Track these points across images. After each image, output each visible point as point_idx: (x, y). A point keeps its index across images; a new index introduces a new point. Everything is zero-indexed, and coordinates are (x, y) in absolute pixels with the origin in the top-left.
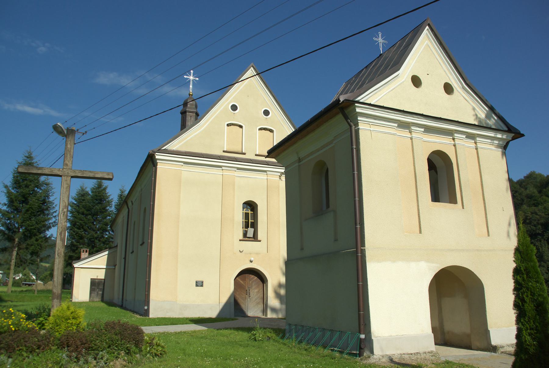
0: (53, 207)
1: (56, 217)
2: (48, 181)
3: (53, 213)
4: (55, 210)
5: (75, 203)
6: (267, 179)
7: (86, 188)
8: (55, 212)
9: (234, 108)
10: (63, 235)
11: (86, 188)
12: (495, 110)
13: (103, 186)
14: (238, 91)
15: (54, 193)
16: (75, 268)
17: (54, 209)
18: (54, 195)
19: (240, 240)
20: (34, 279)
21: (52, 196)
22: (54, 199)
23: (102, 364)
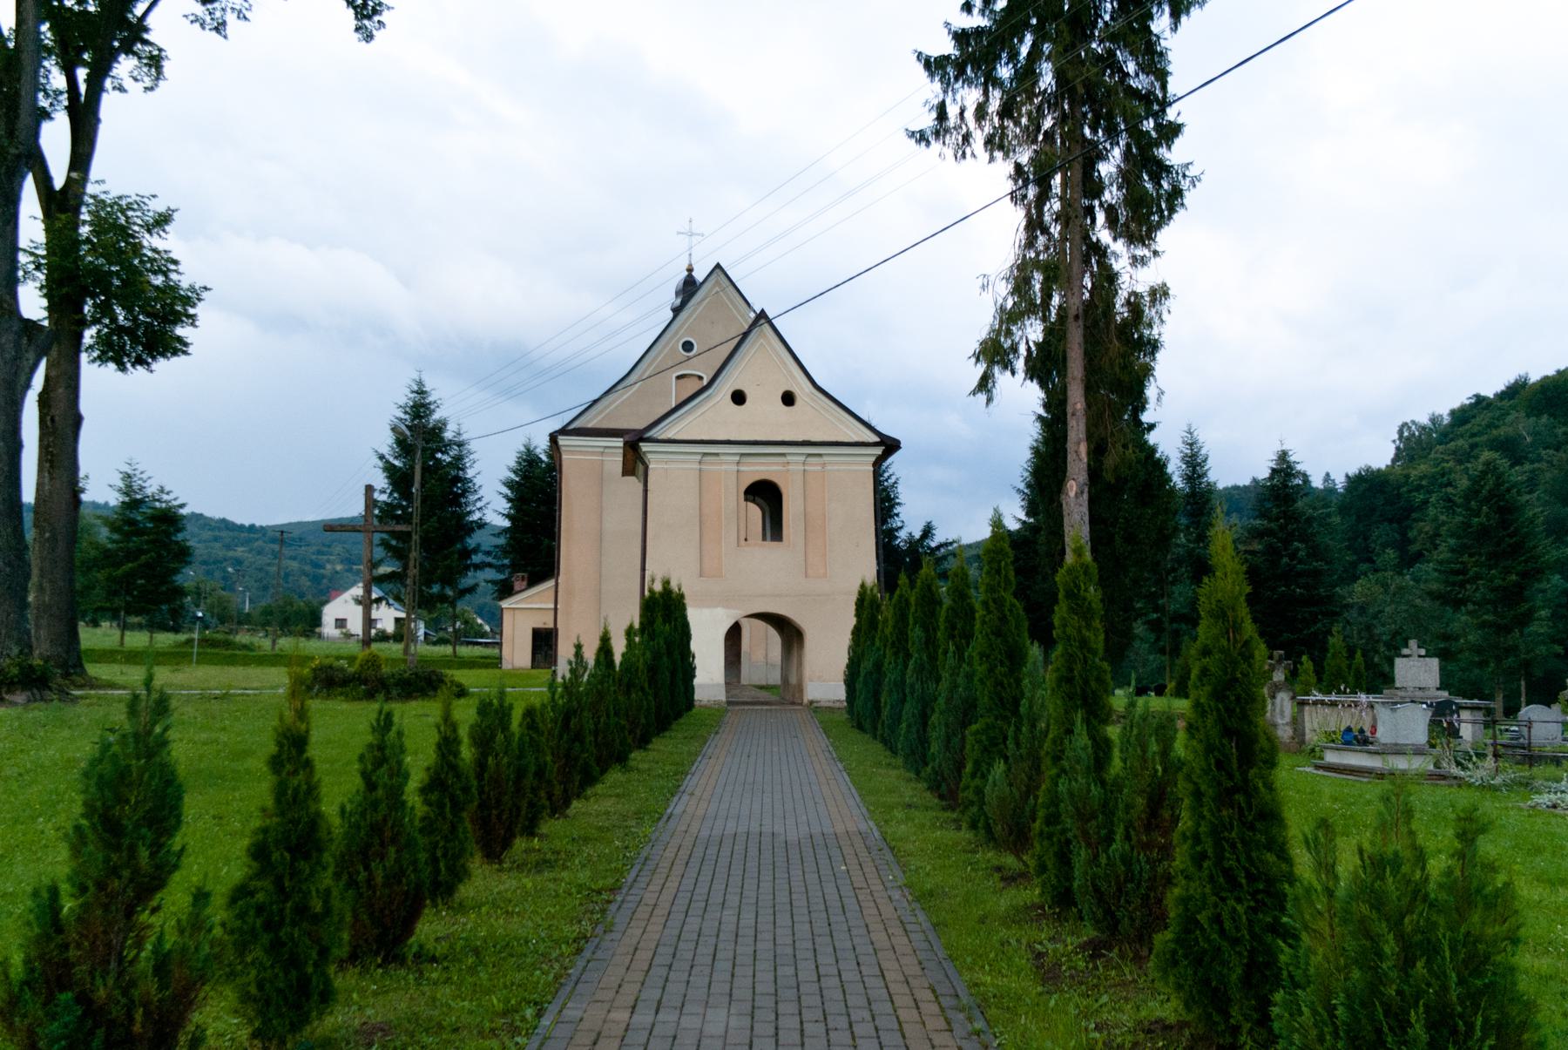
8: (479, 499)
9: (688, 346)
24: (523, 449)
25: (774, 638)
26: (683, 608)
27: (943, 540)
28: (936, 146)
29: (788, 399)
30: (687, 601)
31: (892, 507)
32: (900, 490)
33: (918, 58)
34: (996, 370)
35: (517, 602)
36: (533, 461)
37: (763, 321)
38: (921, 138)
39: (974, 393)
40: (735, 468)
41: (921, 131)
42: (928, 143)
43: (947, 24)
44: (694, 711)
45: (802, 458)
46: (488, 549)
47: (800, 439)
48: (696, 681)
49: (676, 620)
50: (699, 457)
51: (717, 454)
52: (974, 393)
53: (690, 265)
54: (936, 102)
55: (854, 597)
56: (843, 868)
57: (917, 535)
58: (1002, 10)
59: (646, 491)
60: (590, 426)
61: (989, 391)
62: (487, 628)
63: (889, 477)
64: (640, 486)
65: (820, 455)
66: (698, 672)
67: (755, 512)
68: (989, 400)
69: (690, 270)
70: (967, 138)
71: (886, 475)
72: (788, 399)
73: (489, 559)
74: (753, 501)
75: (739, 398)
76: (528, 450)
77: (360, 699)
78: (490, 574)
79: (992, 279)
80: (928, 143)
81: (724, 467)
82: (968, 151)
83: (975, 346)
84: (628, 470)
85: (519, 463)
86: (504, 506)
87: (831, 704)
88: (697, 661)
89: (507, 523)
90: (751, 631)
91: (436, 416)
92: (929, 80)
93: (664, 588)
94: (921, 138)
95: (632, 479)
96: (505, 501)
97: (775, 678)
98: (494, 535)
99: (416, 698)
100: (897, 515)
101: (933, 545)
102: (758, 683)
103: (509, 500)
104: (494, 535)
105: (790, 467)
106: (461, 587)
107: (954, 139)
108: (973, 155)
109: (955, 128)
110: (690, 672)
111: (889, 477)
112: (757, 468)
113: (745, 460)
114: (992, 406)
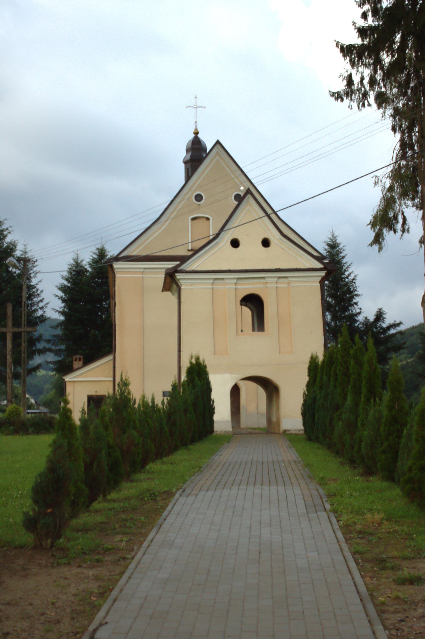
0: (38, 294)
1: (43, 308)
2: (27, 256)
3: (39, 302)
4: (41, 298)
5: (69, 285)
6: (213, 289)
7: (82, 261)
8: (41, 301)
9: (199, 198)
10: (10, 366)
11: (82, 261)
12: (402, 218)
13: (107, 256)
14: (203, 177)
17: (39, 297)
20: (32, 404)
22: (38, 282)
24: (72, 262)
25: (262, 393)
26: (206, 374)
27: (392, 322)
28: (346, 101)
29: (266, 243)
30: (209, 369)
31: (352, 297)
32: (357, 284)
33: (337, 46)
34: (385, 231)
35: (75, 377)
36: (81, 271)
37: (249, 196)
38: (338, 96)
39: (371, 245)
40: (234, 287)
41: (338, 93)
42: (342, 100)
43: (354, 23)
44: (214, 433)
45: (276, 280)
46: (47, 338)
47: (274, 267)
48: (216, 417)
49: (203, 379)
50: (212, 281)
51: (223, 279)
52: (371, 245)
53: (196, 129)
54: (346, 75)
55: (307, 365)
56: (283, 464)
57: (372, 318)
58: (387, 8)
59: (179, 302)
60: (134, 254)
61: (380, 244)
62: (33, 401)
63: (349, 275)
64: (176, 301)
65: (286, 277)
66: (216, 410)
67: (247, 312)
68: (380, 249)
69: (196, 133)
70: (365, 95)
71: (347, 273)
72: (266, 243)
73: (48, 346)
74: (246, 306)
75: (235, 243)
76: (77, 263)
77: (10, 434)
78: (51, 357)
79: (380, 178)
80: (342, 100)
81: (227, 286)
82: (366, 103)
83: (369, 218)
84: (166, 288)
85: (71, 273)
86: (59, 305)
87: (297, 432)
88: (215, 404)
89: (62, 318)
90: (244, 387)
91: (8, 239)
92: (343, 58)
93: (196, 362)
94: (338, 96)
95: (168, 293)
96: (60, 301)
97: (263, 423)
98: (52, 327)
99: (43, 433)
100: (356, 304)
101: (385, 326)
102: (253, 427)
103: (63, 301)
104: (52, 327)
105: (268, 285)
106: (30, 367)
107: (356, 97)
108: (369, 105)
109: (358, 90)
110: (212, 411)
111: (349, 275)
112: (247, 286)
113: (240, 281)
114: (381, 252)
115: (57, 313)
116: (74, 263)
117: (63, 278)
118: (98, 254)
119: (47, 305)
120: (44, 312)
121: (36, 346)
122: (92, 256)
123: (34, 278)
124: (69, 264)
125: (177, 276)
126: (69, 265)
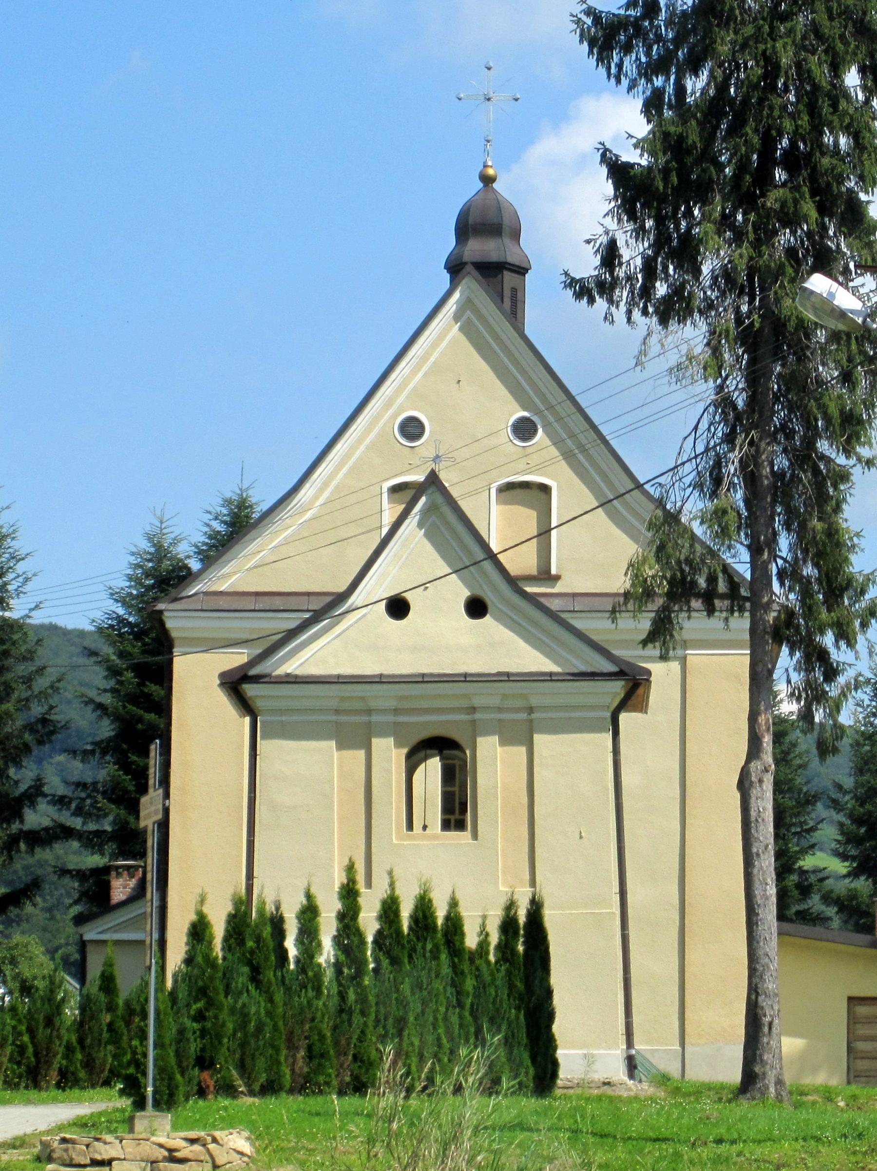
7: (176, 542)
11: (176, 542)
15: (27, 580)
16: (361, 754)
18: (29, 587)
19: (475, 836)
21: (18, 593)
22: (31, 610)
23: (835, 34)
42: (591, 301)
46: (62, 790)
80: (591, 301)
85: (139, 582)
103: (114, 672)
115: (91, 707)
116: (152, 550)
117: (114, 595)
118: (227, 519)
119: (57, 685)
120: (52, 708)
121: (22, 822)
122: (208, 525)
123: (18, 595)
124: (134, 550)
125: (247, 691)
126: (133, 554)
